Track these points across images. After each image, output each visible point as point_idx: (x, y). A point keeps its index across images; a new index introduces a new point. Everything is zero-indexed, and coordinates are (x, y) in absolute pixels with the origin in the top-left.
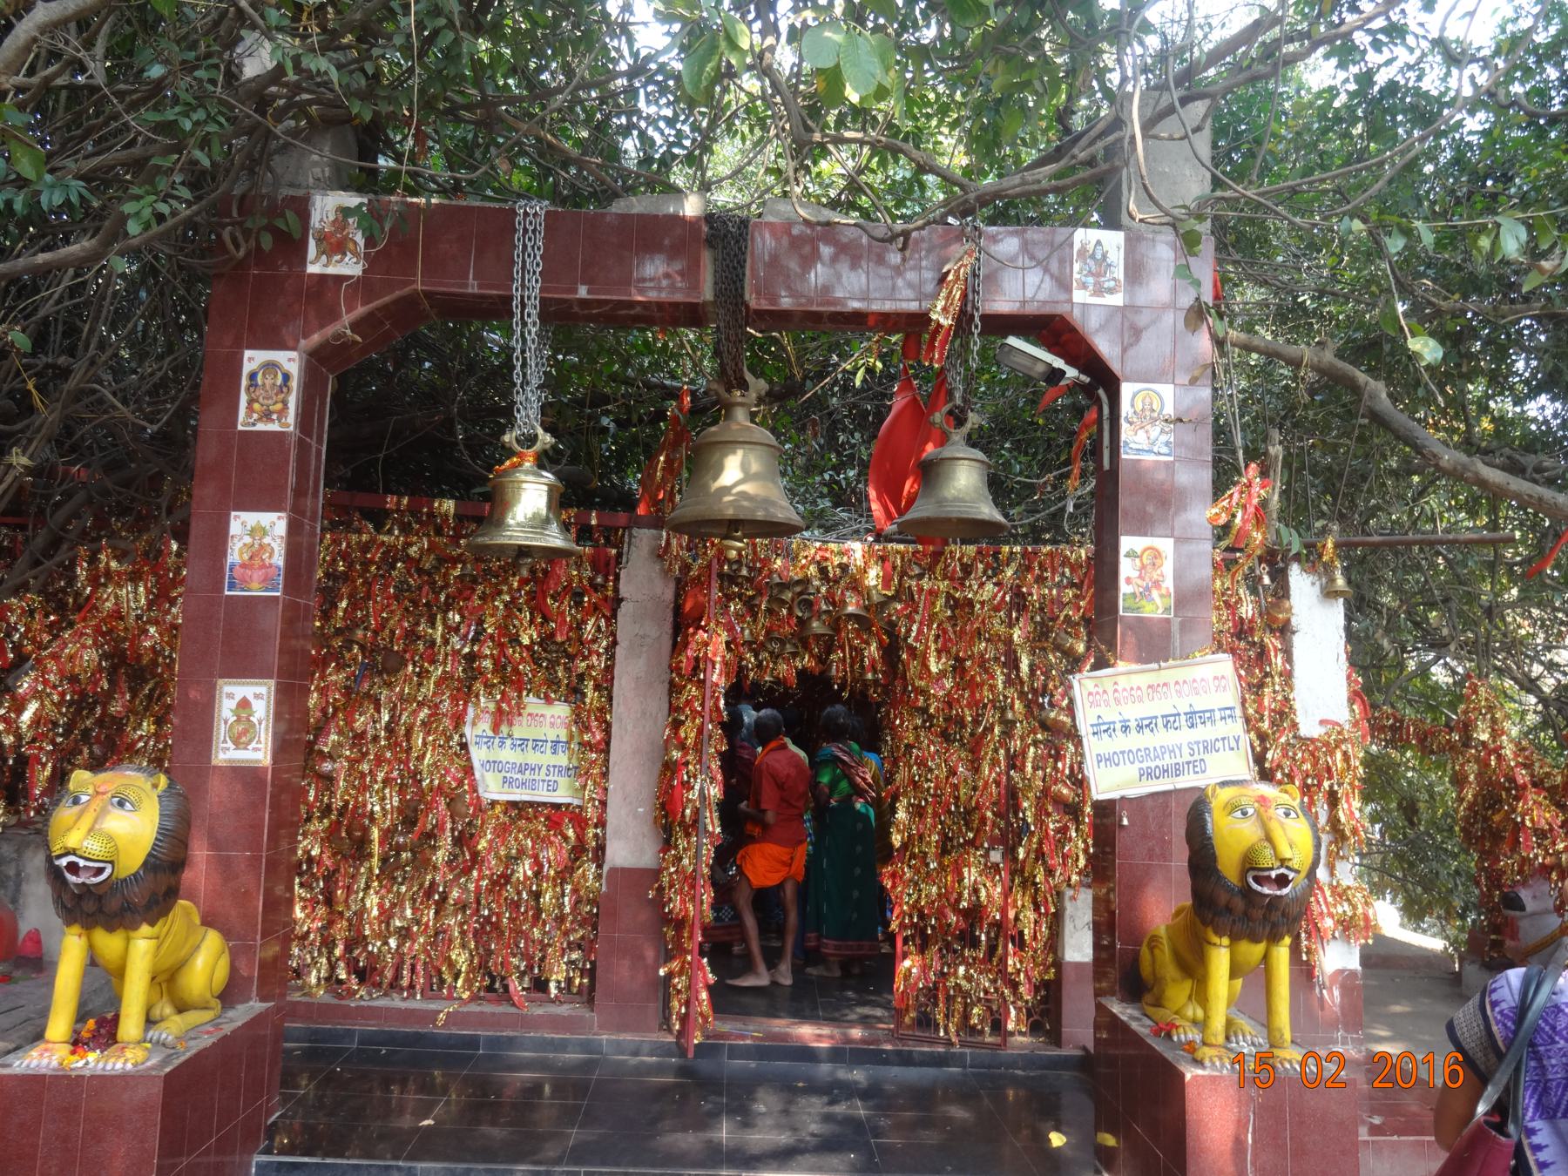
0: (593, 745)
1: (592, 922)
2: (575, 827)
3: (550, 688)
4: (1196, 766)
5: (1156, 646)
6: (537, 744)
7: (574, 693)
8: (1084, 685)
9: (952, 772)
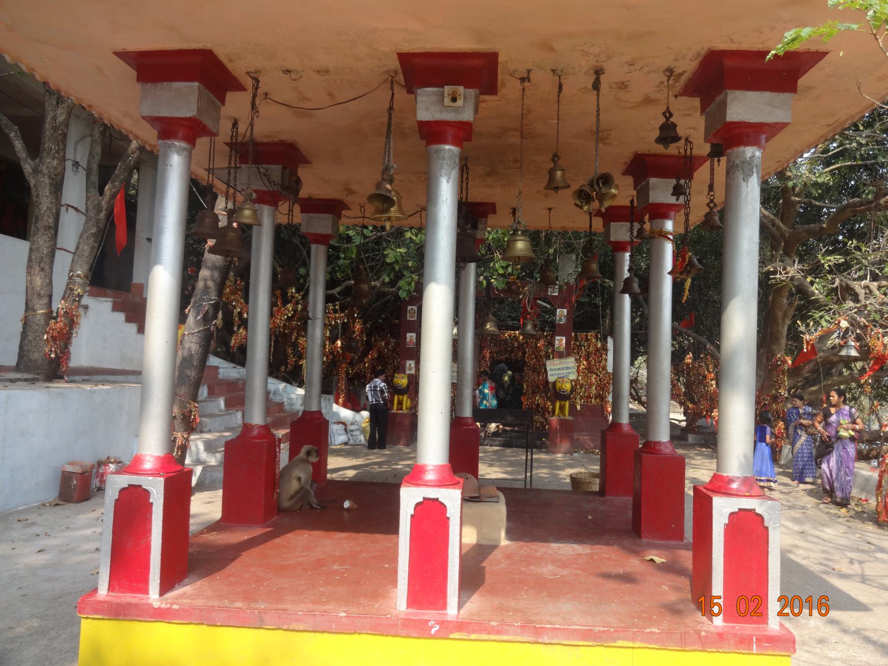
5: (561, 355)
8: (548, 363)
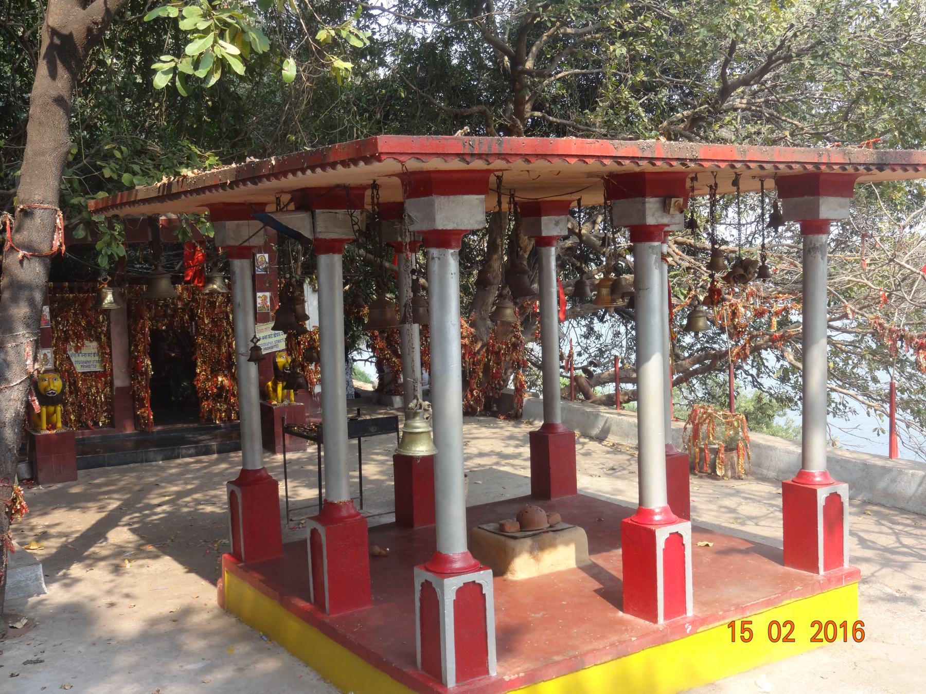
0: (105, 354)
1: (110, 404)
2: (104, 376)
3: (90, 337)
4: (276, 346)
6: (89, 354)
7: (98, 339)
9: (213, 350)
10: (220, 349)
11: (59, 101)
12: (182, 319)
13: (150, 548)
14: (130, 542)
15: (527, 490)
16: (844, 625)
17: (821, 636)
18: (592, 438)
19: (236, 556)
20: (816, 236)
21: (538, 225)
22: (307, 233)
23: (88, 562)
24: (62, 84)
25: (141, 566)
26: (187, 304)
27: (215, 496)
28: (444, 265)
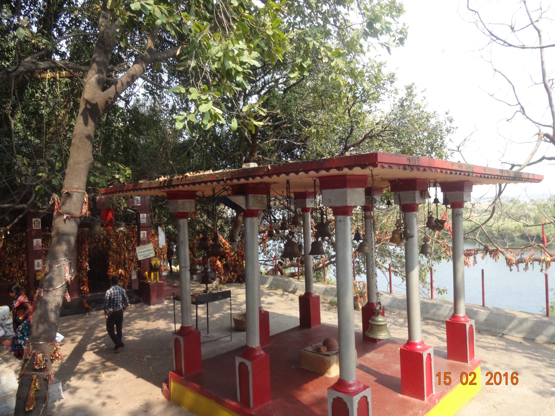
4: (149, 255)
5: (144, 243)
8: (137, 248)
10: (120, 257)
11: (88, 137)
12: (103, 243)
13: (109, 364)
14: (96, 361)
15: (298, 324)
16: (506, 375)
17: (492, 381)
18: (289, 292)
19: (178, 372)
20: (457, 209)
21: (305, 203)
22: (243, 207)
23: (79, 375)
24: (90, 128)
25: (109, 376)
26: (105, 237)
27: (130, 330)
28: (345, 224)
